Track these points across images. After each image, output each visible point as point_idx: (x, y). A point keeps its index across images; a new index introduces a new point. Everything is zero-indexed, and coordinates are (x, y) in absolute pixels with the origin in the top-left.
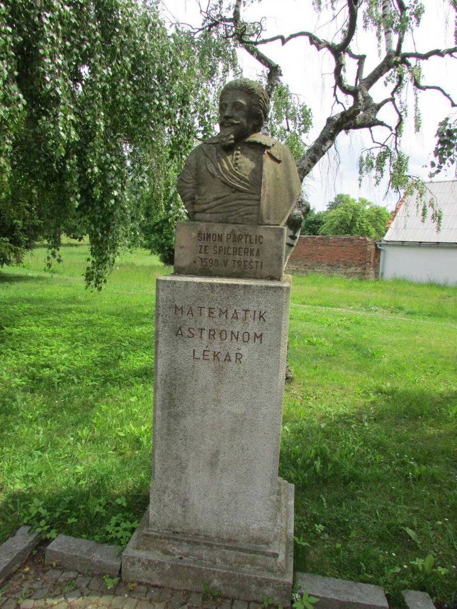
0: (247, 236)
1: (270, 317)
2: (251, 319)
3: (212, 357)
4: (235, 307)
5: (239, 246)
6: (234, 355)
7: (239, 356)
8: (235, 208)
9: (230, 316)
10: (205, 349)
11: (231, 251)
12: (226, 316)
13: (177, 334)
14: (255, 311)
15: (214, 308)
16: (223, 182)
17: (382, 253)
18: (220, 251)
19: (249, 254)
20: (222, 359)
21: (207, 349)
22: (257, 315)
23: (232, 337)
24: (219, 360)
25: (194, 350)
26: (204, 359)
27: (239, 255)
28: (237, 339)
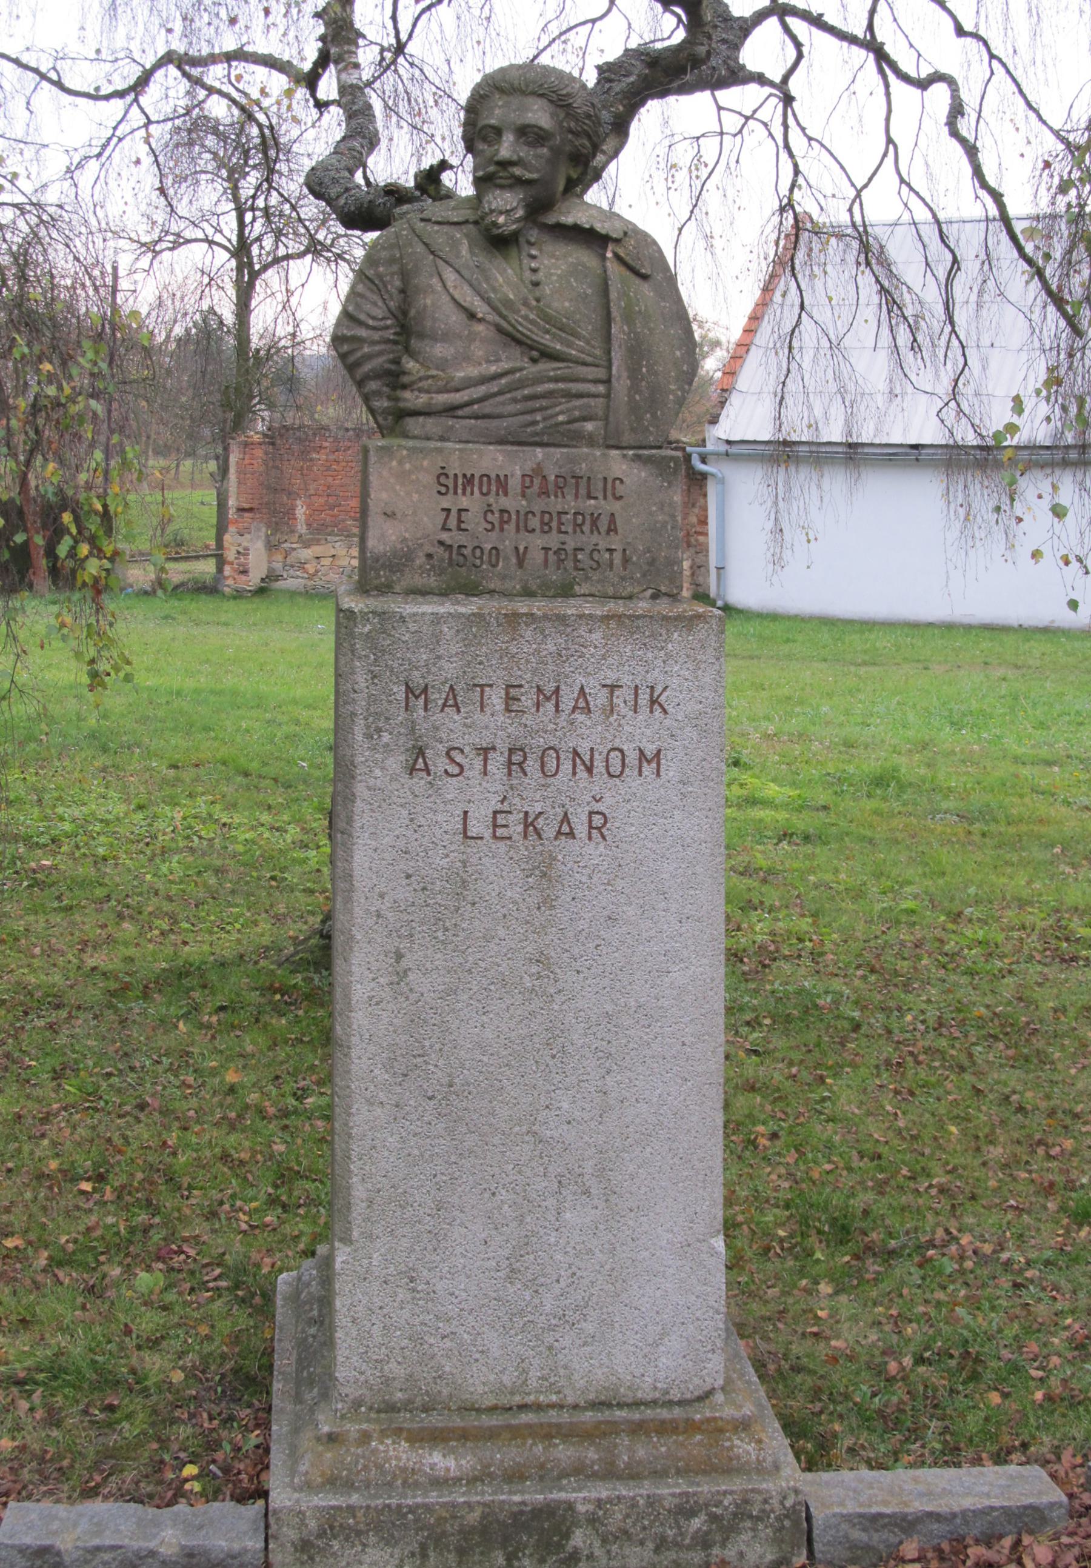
0: (577, 478)
2: (624, 710)
3: (520, 828)
4: (581, 679)
5: (559, 508)
6: (584, 818)
7: (597, 820)
8: (544, 403)
10: (499, 807)
11: (534, 522)
12: (557, 706)
13: (412, 770)
15: (521, 686)
16: (500, 330)
17: (712, 489)
18: (502, 522)
19: (586, 528)
20: (549, 832)
22: (644, 699)
23: (574, 766)
24: (540, 838)
25: (466, 813)
26: (495, 837)
27: (560, 532)
28: (589, 770)
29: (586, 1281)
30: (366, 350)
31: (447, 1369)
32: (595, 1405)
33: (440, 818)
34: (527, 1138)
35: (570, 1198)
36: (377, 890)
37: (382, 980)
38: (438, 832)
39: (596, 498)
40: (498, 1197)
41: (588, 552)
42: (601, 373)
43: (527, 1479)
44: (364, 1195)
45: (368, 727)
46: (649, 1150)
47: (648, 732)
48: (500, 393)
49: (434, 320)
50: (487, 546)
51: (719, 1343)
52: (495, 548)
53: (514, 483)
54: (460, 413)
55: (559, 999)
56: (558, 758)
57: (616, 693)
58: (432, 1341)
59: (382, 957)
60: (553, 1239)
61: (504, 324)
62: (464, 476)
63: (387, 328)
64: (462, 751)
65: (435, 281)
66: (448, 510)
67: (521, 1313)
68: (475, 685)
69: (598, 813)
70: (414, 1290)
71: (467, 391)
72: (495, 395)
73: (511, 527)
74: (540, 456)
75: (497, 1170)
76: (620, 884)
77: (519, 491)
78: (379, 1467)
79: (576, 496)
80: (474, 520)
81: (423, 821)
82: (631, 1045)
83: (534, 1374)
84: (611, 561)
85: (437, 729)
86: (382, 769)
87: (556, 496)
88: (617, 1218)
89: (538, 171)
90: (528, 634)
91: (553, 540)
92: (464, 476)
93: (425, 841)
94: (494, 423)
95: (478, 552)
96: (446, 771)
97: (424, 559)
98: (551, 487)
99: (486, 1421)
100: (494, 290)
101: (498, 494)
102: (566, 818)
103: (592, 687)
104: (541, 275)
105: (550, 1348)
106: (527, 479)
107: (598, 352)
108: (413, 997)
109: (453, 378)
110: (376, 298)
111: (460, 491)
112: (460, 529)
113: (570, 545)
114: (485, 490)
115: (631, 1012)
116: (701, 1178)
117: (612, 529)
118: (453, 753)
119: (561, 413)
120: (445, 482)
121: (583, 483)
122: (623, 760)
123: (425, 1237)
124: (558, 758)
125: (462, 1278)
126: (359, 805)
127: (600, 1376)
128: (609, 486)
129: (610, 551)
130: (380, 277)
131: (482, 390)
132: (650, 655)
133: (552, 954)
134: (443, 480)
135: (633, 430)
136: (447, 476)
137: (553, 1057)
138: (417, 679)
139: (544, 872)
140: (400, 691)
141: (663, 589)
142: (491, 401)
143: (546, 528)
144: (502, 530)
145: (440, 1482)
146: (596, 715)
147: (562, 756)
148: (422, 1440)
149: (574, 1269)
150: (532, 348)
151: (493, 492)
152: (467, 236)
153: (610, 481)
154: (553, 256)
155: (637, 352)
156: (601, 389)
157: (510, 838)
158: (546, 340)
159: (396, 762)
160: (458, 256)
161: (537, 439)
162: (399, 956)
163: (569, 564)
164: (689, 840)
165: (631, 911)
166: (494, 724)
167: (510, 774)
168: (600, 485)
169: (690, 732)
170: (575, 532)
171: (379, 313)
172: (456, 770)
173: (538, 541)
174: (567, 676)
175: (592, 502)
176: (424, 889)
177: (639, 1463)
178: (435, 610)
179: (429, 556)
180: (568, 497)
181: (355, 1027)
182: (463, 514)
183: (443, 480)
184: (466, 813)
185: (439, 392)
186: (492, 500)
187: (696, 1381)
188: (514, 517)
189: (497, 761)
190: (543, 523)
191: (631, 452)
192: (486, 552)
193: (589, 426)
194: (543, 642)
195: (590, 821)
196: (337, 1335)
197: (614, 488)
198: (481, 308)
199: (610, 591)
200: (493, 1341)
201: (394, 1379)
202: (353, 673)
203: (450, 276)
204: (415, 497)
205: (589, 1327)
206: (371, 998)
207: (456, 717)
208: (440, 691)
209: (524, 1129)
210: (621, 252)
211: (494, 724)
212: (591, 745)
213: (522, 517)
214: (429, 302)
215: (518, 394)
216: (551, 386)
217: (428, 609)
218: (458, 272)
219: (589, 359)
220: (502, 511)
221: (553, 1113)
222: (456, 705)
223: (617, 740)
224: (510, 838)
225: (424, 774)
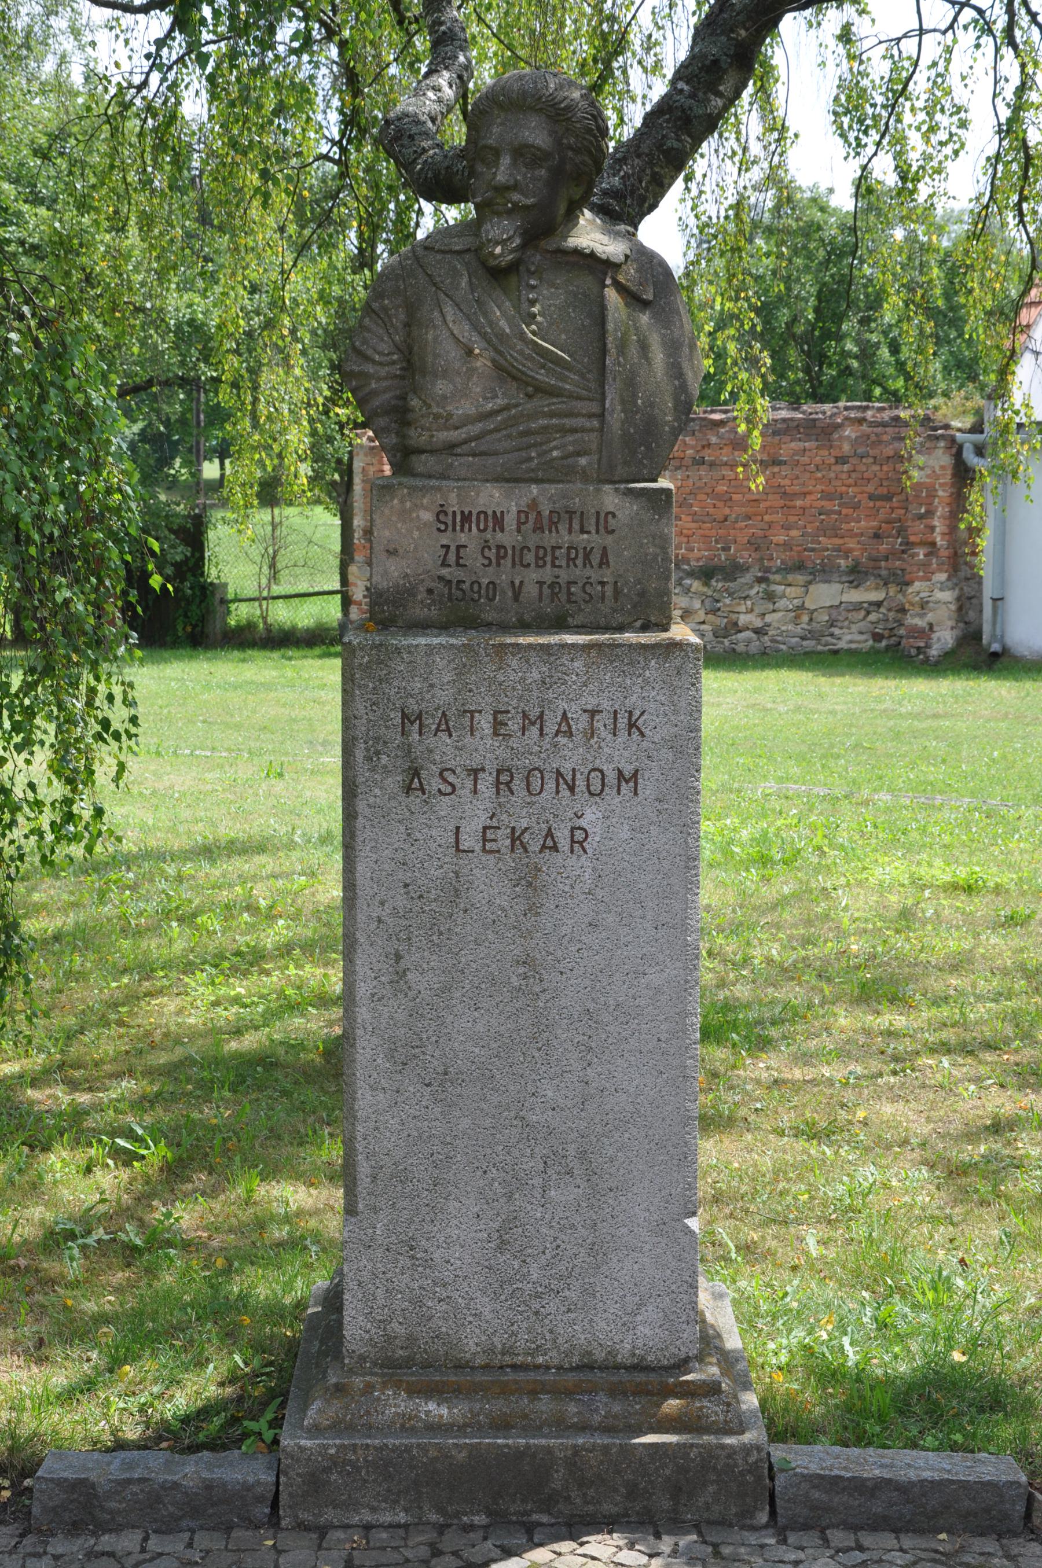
0: (571, 513)
5: (553, 543)
6: (567, 832)
7: (579, 835)
10: (488, 823)
11: (529, 557)
12: (541, 730)
13: (408, 790)
14: (615, 712)
15: (508, 712)
18: (499, 558)
19: (579, 562)
20: (535, 847)
22: (623, 722)
24: (526, 851)
25: (458, 828)
26: (484, 850)
28: (572, 789)
29: (570, 1253)
31: (444, 1330)
33: (434, 833)
34: (515, 1123)
35: (554, 1177)
36: (378, 898)
37: (383, 979)
38: (433, 846)
39: (589, 532)
40: (489, 1175)
41: (580, 585)
42: (595, 408)
43: (513, 1427)
44: (368, 1171)
45: (367, 750)
46: (627, 1135)
47: (626, 753)
48: (497, 430)
49: (436, 356)
50: (485, 581)
52: (492, 583)
54: (459, 450)
56: (542, 778)
57: (597, 718)
58: (430, 1304)
59: (383, 958)
60: (539, 1215)
61: (502, 361)
62: (462, 512)
63: (394, 363)
64: (454, 772)
66: (447, 547)
68: (465, 711)
69: (580, 828)
70: (413, 1257)
71: (465, 429)
72: (491, 432)
74: (535, 491)
75: (489, 1151)
77: (514, 527)
79: (570, 532)
80: (473, 557)
81: (418, 835)
82: (610, 1041)
84: (603, 593)
85: (431, 751)
86: (381, 788)
87: (550, 531)
88: (598, 1196)
90: (514, 663)
91: (547, 574)
92: (462, 512)
93: (421, 854)
94: (491, 460)
95: (476, 587)
96: (439, 790)
97: (425, 595)
98: (545, 522)
99: (480, 1377)
101: (494, 530)
102: (549, 834)
103: (574, 711)
105: (537, 1313)
106: (523, 515)
107: (592, 385)
111: (458, 528)
112: (458, 564)
114: (482, 527)
115: (611, 1009)
116: (675, 1162)
117: (604, 562)
118: (446, 774)
119: (556, 448)
122: (603, 780)
123: (424, 1210)
124: (542, 778)
125: (457, 1247)
127: (582, 1341)
128: (602, 521)
129: (602, 584)
130: (385, 309)
131: (478, 427)
132: (628, 681)
133: (538, 956)
134: (442, 517)
136: (446, 514)
137: (539, 1049)
138: (413, 706)
139: (529, 881)
140: (396, 717)
141: (653, 619)
142: (488, 438)
143: (541, 563)
144: (498, 564)
145: (434, 1428)
146: (578, 738)
147: (547, 776)
148: (419, 1392)
149: (559, 1242)
150: (527, 384)
151: (490, 529)
152: (467, 265)
153: (602, 515)
154: (553, 285)
156: (596, 423)
157: (498, 851)
158: (542, 376)
159: (394, 782)
161: (532, 475)
162: (398, 957)
163: (563, 597)
164: (665, 854)
165: (611, 918)
166: (484, 747)
167: (498, 793)
168: (593, 521)
169: (666, 754)
170: (568, 566)
171: (384, 347)
172: (449, 789)
173: (533, 575)
174: (550, 702)
175: (585, 536)
176: (421, 897)
177: (616, 1417)
178: (429, 641)
179: (430, 591)
181: (359, 1020)
182: (462, 550)
183: (442, 517)
184: (458, 828)
188: (510, 552)
189: (485, 783)
190: (537, 558)
191: (622, 486)
192: (484, 586)
193: (583, 461)
195: (572, 836)
196: (345, 1297)
197: (606, 522)
201: (396, 1338)
204: (416, 534)
206: (373, 995)
207: (448, 741)
208: (433, 717)
209: (513, 1114)
212: (573, 765)
213: (517, 553)
217: (422, 641)
220: (499, 547)
221: (539, 1100)
222: (448, 729)
223: (598, 761)
224: (498, 851)
225: (419, 793)
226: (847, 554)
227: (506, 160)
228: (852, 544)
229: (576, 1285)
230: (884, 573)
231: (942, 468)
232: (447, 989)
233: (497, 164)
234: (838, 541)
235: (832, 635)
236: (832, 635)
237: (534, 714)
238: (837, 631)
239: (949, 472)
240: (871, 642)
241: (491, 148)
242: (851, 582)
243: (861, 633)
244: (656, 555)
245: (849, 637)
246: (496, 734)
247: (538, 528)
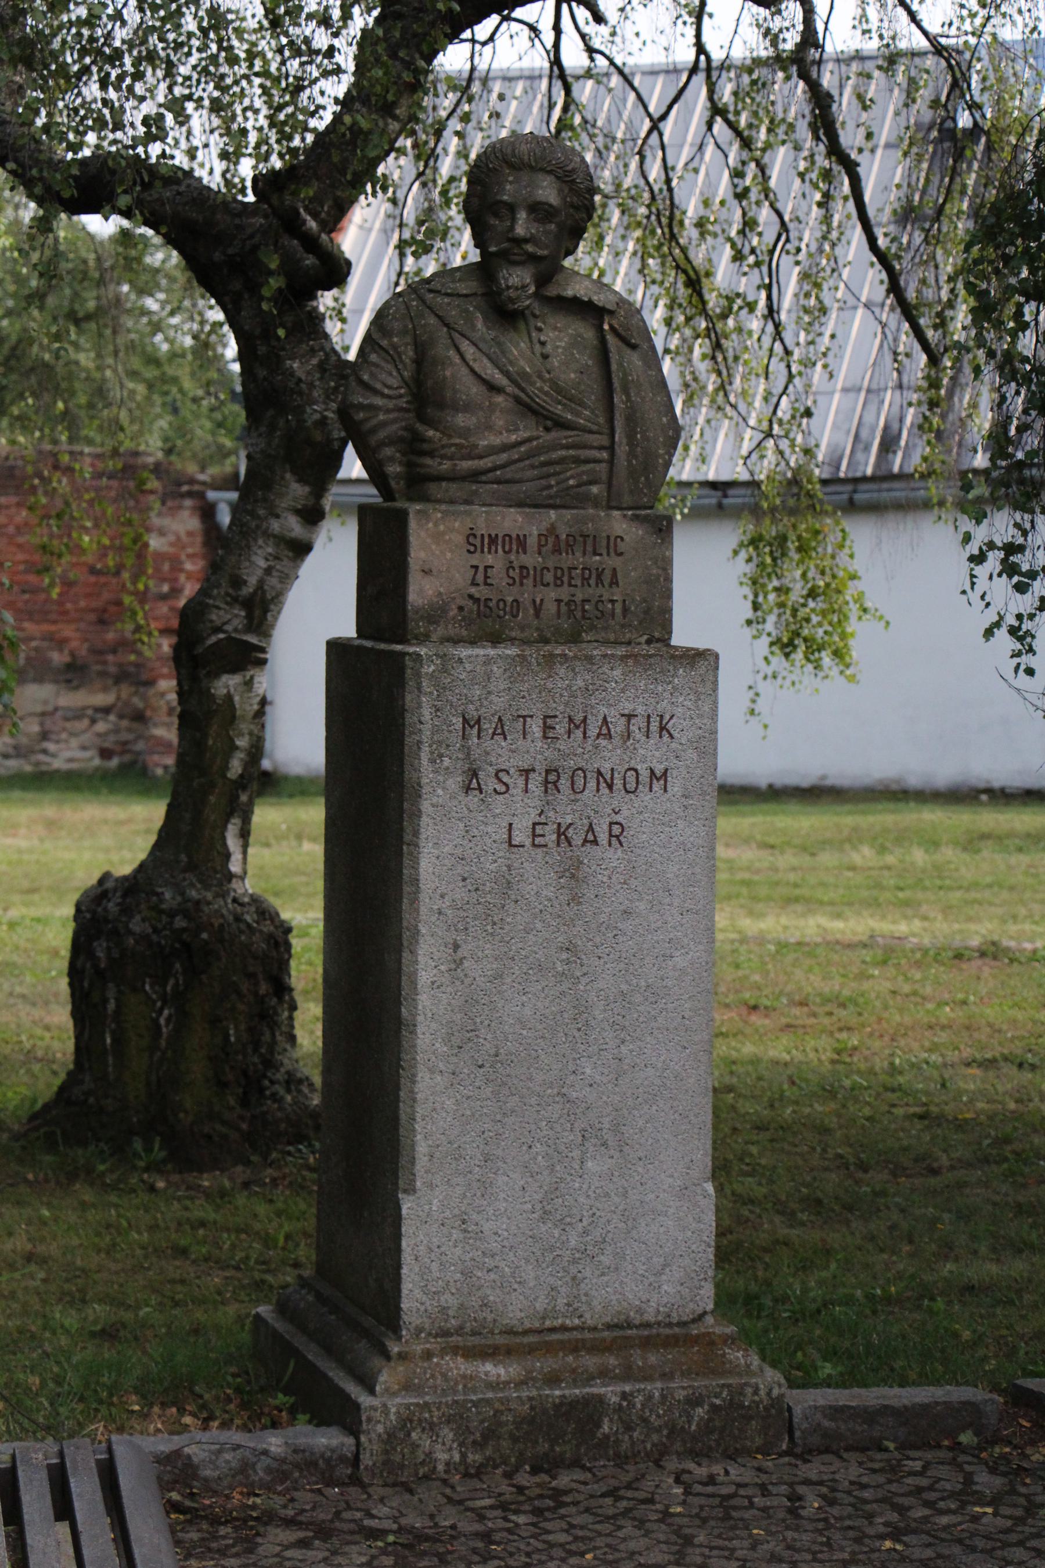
0: (585, 537)
1: (682, 727)
2: (638, 735)
3: (554, 837)
4: (604, 710)
5: (569, 564)
6: (606, 827)
7: (616, 830)
8: (558, 468)
9: (593, 731)
10: (538, 819)
11: (549, 577)
13: (468, 789)
16: (518, 401)
19: (592, 582)
20: (578, 841)
21: (543, 820)
22: (654, 726)
26: (534, 845)
28: (610, 787)
30: (381, 417)
32: (609, 1327)
33: (490, 829)
40: (534, 1150)
42: (605, 441)
48: (519, 460)
49: (455, 391)
50: (510, 599)
51: (711, 1273)
53: (532, 542)
55: (584, 980)
61: (522, 395)
63: (401, 396)
65: (452, 353)
66: (476, 567)
67: (552, 1248)
70: (465, 1231)
73: (529, 582)
76: (633, 883)
78: (444, 1376)
80: (498, 575)
83: (561, 1301)
89: (547, 247)
90: (562, 672)
91: (564, 593)
93: (478, 849)
94: (515, 488)
98: (563, 545)
100: (511, 363)
102: (591, 828)
104: (549, 348)
107: (601, 420)
108: (467, 981)
109: (476, 446)
110: (390, 367)
113: (579, 597)
117: (614, 582)
120: (474, 542)
121: (590, 541)
123: (475, 1184)
126: (425, 820)
129: (613, 602)
130: (395, 347)
131: (504, 457)
135: (631, 492)
138: (472, 712)
139: (573, 874)
140: (458, 722)
146: (617, 741)
150: (546, 418)
154: (555, 328)
155: (632, 420)
156: (605, 455)
158: (559, 409)
159: (454, 783)
160: (473, 327)
162: (456, 947)
165: (642, 906)
168: (604, 543)
171: (394, 382)
172: (503, 789)
173: (552, 594)
179: (461, 608)
180: (578, 554)
185: (463, 458)
186: (513, 557)
187: (691, 1305)
190: (556, 578)
193: (595, 489)
194: (574, 678)
198: (499, 378)
199: (612, 637)
200: (529, 1273)
202: (420, 707)
203: (469, 351)
204: (449, 555)
205: (606, 1260)
210: (615, 323)
211: (534, 750)
214: (448, 373)
215: (536, 461)
216: (563, 453)
218: (475, 345)
219: (595, 428)
220: (522, 567)
222: (503, 733)
226: (60, 643)
227: (522, 215)
228: (68, 631)
229: (609, 1250)
230: (112, 669)
231: (190, 534)
232: (499, 976)
233: (514, 220)
234: (46, 627)
235: (45, 752)
236: (45, 752)
237: (578, 718)
238: (51, 747)
239: (199, 539)
240: (97, 762)
241: (505, 203)
242: (69, 681)
243: (84, 748)
244: (658, 576)
245: (68, 754)
246: (545, 737)
247: (557, 550)
